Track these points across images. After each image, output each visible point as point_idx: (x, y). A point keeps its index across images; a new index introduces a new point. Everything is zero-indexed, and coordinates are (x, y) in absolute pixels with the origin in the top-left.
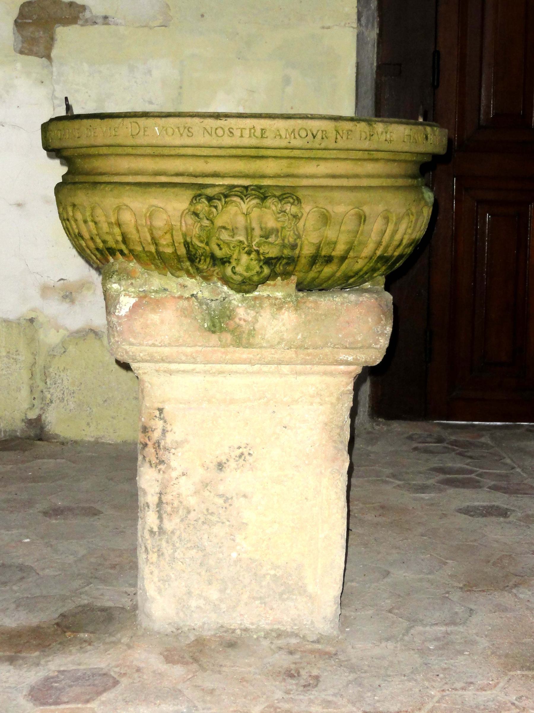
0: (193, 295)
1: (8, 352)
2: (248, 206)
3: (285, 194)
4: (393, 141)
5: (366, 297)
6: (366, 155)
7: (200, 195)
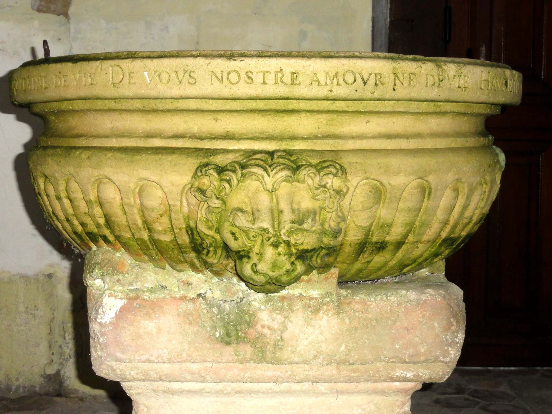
0: (199, 295)
1: (27, 308)
2: (274, 180)
3: (324, 162)
4: (467, 88)
5: (431, 295)
6: (431, 107)
7: (207, 165)
